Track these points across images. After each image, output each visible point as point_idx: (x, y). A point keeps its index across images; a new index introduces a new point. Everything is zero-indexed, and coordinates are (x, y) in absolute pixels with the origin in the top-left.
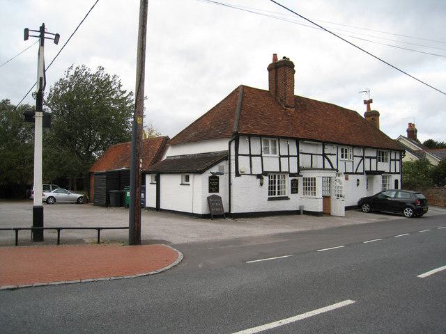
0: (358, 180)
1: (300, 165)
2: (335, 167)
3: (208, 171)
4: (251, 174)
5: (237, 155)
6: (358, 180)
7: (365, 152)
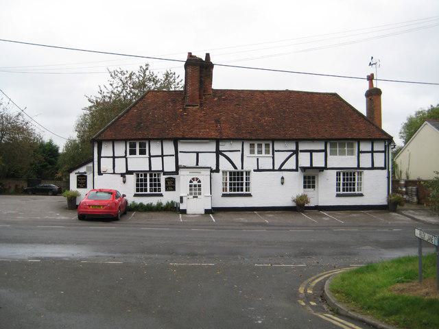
0: (283, 178)
1: (179, 164)
2: (239, 169)
3: (77, 171)
4: (114, 173)
5: (100, 157)
6: (283, 178)
7: (375, 144)
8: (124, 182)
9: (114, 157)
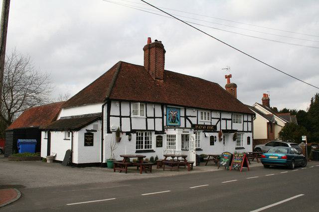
5: (109, 116)
7: (187, 110)
8: (130, 140)
9: (154, 118)
